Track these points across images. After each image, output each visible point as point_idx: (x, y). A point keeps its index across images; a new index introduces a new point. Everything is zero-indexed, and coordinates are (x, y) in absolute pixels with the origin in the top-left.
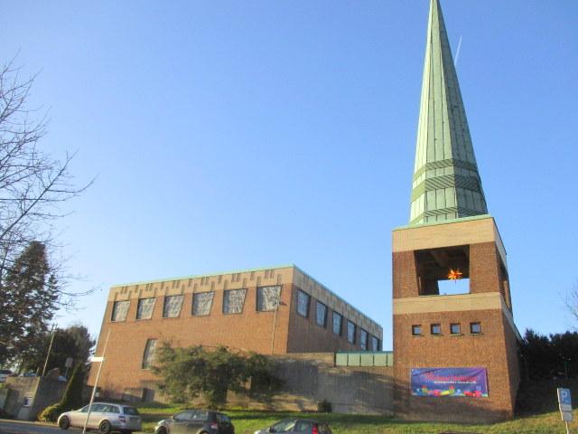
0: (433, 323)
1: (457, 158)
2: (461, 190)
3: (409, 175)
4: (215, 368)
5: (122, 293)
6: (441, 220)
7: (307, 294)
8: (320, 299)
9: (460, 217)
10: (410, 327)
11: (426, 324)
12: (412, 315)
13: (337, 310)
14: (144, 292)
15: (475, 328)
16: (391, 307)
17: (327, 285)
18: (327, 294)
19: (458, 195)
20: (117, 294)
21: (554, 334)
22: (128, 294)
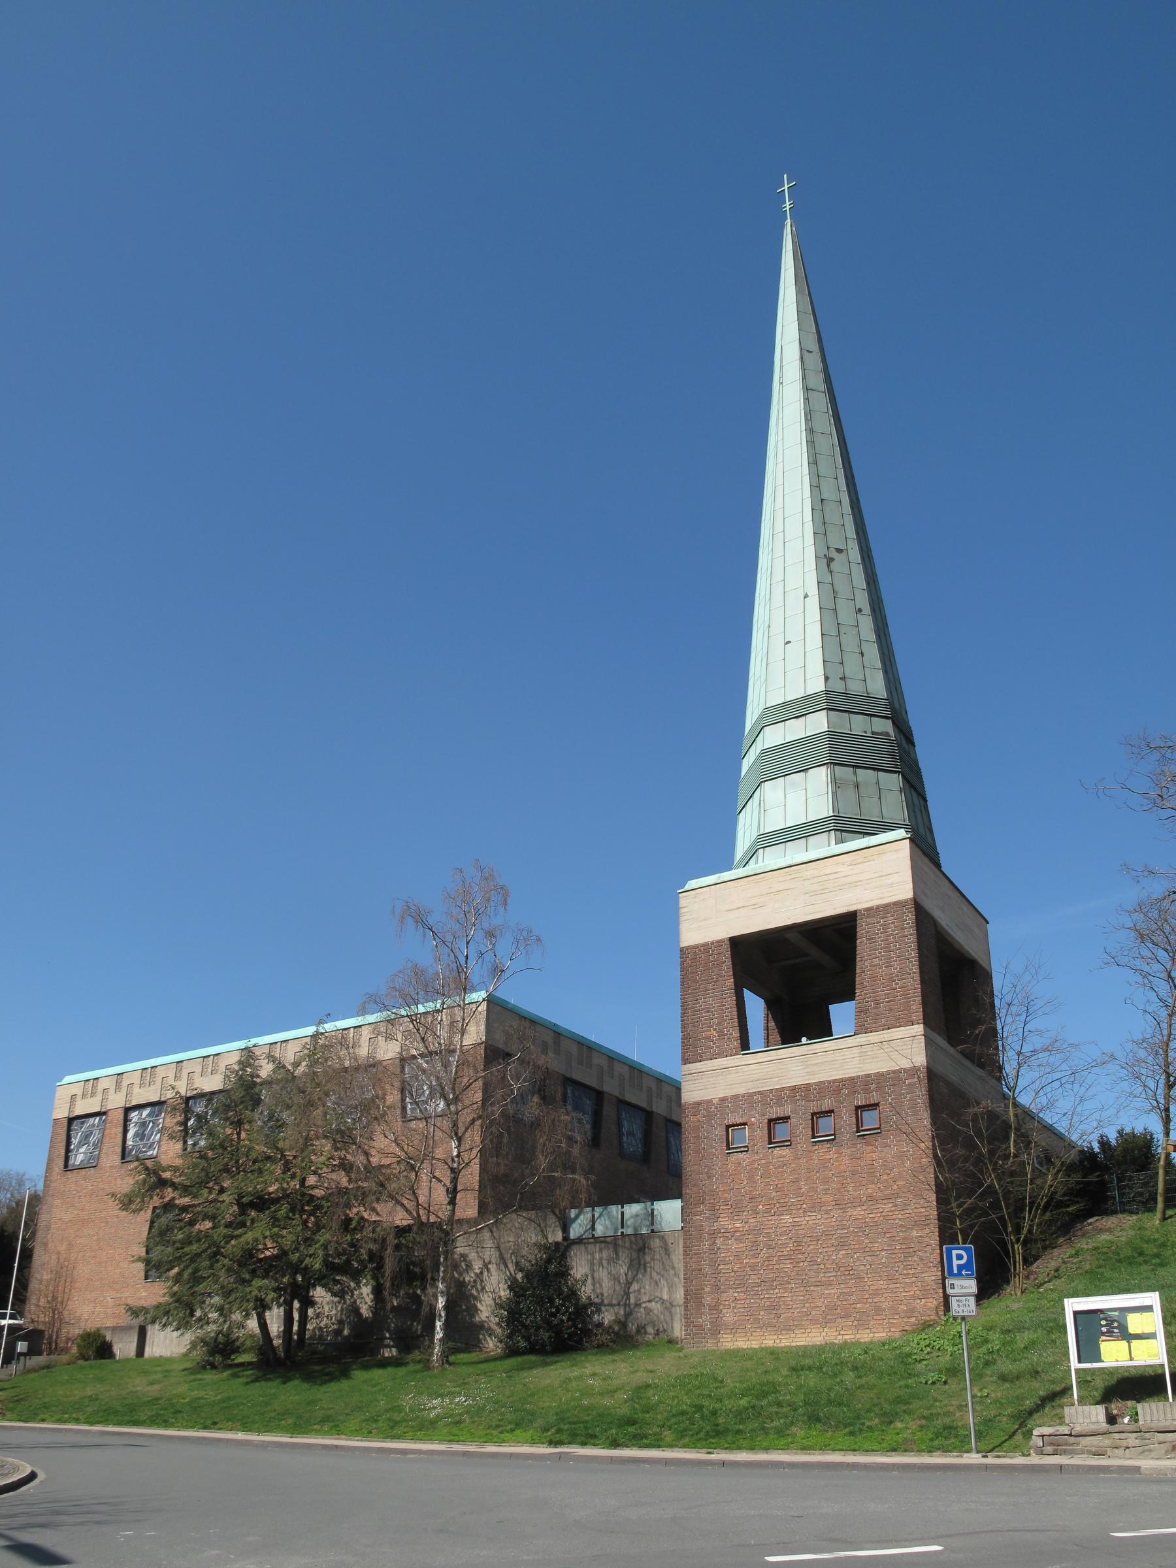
0: (813, 1108)
1: (839, 687)
2: (844, 773)
3: (247, 1037)
4: (417, 1351)
5: (84, 1096)
6: (796, 852)
7: (69, 1130)
8: (576, 1076)
9: (842, 841)
10: (721, 1131)
11: (758, 1120)
12: (723, 1100)
13: (632, 1097)
14: (136, 1090)
15: (870, 1119)
16: (51, 1129)
17: (593, 1036)
18: (597, 1060)
19: (837, 785)
20: (73, 1097)
21: (1128, 1130)
22: (99, 1097)
